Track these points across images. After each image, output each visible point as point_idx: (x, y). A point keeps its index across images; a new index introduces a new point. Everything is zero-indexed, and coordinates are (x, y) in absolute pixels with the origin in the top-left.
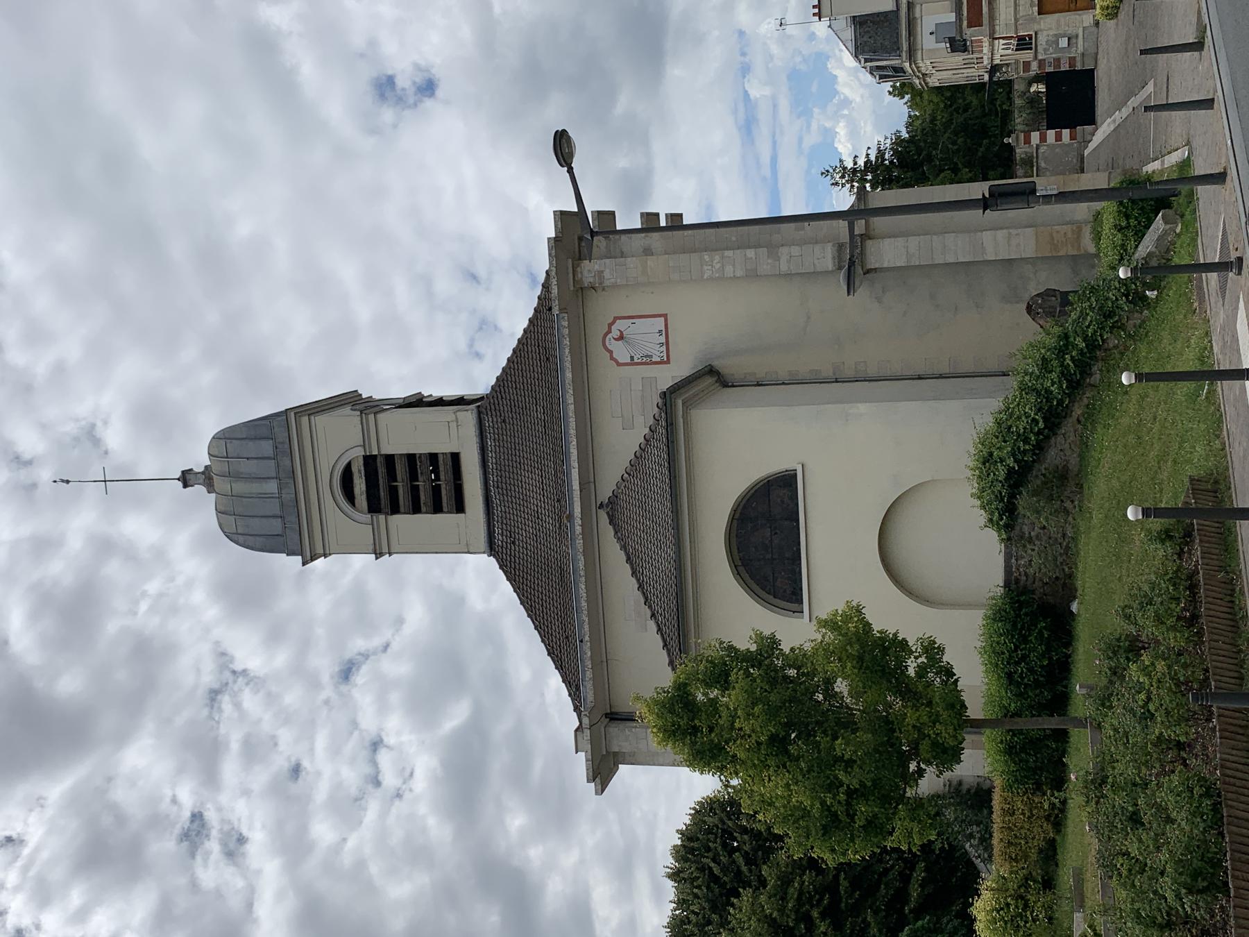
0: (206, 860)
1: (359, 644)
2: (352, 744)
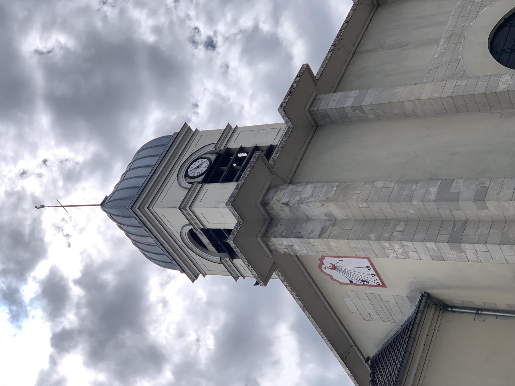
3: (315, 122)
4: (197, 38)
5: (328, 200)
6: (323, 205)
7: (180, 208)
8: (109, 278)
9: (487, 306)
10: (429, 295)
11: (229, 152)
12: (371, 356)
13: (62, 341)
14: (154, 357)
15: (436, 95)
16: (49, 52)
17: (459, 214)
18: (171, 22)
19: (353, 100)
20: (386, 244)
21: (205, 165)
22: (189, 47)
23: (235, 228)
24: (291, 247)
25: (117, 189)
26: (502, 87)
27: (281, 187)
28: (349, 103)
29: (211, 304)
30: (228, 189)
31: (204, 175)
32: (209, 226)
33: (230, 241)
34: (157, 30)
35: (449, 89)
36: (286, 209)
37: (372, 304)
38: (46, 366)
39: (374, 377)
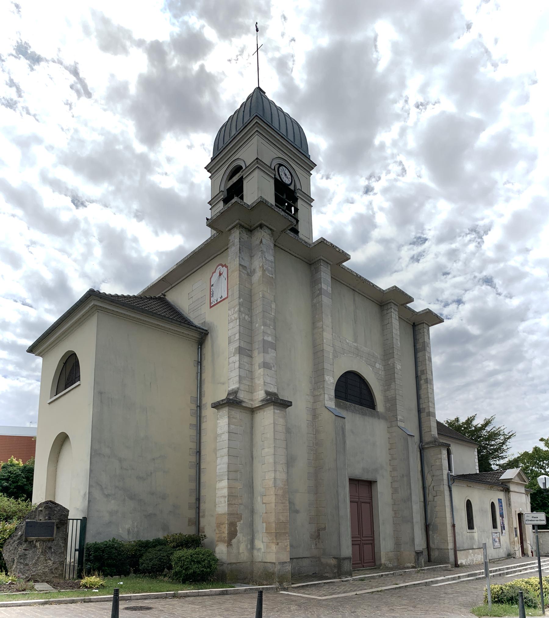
0: (409, 250)
1: (498, 282)
2: (458, 291)
3: (313, 263)
4: (373, 179)
5: (264, 271)
6: (260, 267)
7: (257, 159)
8: (206, 98)
9: (203, 368)
10: (207, 334)
11: (295, 200)
12: (166, 297)
13: (156, 51)
14: (151, 137)
15: (325, 341)
16: (376, 46)
17: (256, 353)
18: (385, 158)
19: (325, 288)
20: (237, 309)
21: (287, 181)
22: (367, 173)
23: (245, 203)
24: (234, 245)
25: (271, 103)
26: (327, 378)
27: (272, 238)
28: (324, 286)
29: (192, 186)
30: (271, 199)
31: (279, 179)
32: (245, 182)
33: (235, 199)
34: (382, 147)
35: (328, 348)
36: (258, 242)
37: (199, 299)
38: (136, 36)
39: (154, 299)
